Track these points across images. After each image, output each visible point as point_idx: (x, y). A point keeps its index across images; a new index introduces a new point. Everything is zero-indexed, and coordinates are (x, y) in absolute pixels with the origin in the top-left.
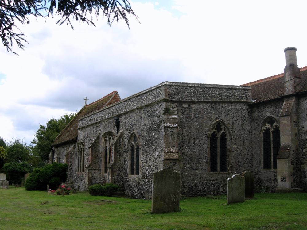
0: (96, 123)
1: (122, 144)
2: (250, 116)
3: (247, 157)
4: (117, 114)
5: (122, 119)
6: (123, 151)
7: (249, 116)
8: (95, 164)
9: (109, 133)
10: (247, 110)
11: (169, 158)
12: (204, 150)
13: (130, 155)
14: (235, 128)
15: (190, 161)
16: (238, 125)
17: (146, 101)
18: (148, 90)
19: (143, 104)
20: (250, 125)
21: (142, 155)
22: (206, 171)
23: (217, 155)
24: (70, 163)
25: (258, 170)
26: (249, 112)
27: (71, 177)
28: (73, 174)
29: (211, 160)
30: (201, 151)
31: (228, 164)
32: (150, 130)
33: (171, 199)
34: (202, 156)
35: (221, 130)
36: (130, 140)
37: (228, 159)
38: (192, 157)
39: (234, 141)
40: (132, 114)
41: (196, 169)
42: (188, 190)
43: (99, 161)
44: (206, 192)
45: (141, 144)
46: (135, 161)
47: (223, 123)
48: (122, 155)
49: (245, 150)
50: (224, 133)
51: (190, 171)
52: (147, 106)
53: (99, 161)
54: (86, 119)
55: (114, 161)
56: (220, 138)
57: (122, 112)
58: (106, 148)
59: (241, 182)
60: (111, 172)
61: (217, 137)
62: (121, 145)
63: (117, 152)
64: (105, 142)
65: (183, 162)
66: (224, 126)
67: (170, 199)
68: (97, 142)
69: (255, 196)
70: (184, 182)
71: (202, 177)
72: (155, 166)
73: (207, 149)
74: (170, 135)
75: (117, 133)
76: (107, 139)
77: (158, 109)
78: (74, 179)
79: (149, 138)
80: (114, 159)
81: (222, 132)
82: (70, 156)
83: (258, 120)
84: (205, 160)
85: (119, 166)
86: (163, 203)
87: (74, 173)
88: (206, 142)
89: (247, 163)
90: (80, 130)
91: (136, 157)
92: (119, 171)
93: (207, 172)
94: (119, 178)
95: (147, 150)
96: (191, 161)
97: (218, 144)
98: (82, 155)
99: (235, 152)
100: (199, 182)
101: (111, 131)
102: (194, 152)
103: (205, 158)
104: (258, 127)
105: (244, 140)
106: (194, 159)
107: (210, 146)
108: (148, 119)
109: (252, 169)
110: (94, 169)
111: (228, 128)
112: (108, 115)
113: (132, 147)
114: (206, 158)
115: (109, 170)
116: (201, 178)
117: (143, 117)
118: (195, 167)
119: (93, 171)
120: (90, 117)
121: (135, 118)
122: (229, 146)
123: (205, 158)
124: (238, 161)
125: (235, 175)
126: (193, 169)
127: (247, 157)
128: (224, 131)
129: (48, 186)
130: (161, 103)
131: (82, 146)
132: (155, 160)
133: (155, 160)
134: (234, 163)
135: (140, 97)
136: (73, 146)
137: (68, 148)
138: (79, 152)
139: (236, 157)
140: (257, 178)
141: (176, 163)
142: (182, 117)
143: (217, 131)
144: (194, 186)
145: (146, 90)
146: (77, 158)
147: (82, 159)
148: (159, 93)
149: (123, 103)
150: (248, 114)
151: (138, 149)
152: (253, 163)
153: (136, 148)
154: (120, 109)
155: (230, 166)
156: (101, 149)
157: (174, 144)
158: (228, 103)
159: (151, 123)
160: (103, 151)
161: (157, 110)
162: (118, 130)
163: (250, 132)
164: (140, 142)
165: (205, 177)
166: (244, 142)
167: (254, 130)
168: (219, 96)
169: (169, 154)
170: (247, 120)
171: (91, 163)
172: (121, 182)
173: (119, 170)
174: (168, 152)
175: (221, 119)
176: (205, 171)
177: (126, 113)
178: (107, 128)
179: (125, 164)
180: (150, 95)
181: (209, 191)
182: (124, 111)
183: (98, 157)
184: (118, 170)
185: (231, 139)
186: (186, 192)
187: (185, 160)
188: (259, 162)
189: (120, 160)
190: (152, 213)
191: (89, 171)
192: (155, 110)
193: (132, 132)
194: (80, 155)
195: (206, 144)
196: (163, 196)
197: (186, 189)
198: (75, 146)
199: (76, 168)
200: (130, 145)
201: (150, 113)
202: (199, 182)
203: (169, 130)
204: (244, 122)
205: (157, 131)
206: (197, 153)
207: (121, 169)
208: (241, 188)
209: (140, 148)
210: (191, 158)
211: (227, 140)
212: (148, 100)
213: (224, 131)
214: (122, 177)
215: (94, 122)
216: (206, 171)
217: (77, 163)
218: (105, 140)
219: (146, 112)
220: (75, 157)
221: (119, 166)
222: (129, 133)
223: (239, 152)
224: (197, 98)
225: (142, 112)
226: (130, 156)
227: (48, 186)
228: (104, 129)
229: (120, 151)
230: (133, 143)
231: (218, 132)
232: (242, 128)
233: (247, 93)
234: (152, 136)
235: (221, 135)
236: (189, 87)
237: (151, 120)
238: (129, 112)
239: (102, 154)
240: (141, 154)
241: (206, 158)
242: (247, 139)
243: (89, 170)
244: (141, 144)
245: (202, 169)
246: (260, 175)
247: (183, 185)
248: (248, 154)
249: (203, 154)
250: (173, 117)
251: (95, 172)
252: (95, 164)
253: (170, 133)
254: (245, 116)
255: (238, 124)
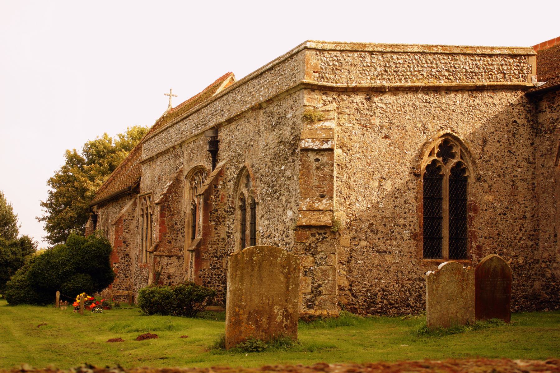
0: (174, 147)
1: (221, 193)
2: (532, 120)
3: (522, 224)
4: (212, 124)
5: (223, 135)
6: (225, 210)
7: (528, 121)
8: (170, 242)
9: (199, 171)
10: (524, 106)
11: (308, 223)
12: (407, 205)
13: (239, 220)
14: (489, 153)
15: (369, 233)
16: (498, 144)
17: (269, 90)
18: (271, 64)
19: (262, 97)
20: (532, 144)
21: (261, 218)
22: (411, 257)
23: (441, 218)
24: (125, 242)
25: (549, 255)
26: (529, 112)
27: (128, 275)
28: (131, 269)
29: (425, 231)
30: (398, 209)
31: (469, 240)
32: (276, 157)
33: (290, 321)
34: (402, 221)
35: (453, 156)
36: (237, 184)
37: (470, 229)
38: (375, 223)
39: (486, 185)
40: (243, 122)
41: (385, 252)
42: (365, 302)
43: (180, 235)
44: (412, 307)
45: (258, 192)
46: (248, 232)
47: (457, 139)
48: (223, 221)
49: (517, 206)
50: (459, 164)
51: (369, 257)
52: (269, 101)
53: (180, 235)
54: (156, 138)
55: (203, 233)
56: (450, 177)
57: (222, 120)
58: (194, 205)
59: (462, 280)
60: (196, 261)
61: (441, 173)
62: (220, 198)
63: (211, 213)
64: (192, 190)
65: (351, 235)
66: (459, 147)
67: (271, 318)
68: (176, 192)
69: (513, 319)
70: (353, 282)
71: (401, 272)
72: (286, 245)
73: (415, 204)
74: (314, 168)
75: (213, 169)
76: (196, 184)
77: (292, 108)
78: (132, 280)
79: (274, 179)
80: (203, 230)
81: (455, 161)
82: (124, 227)
83: (551, 132)
84: (408, 230)
85: (214, 247)
86: (253, 326)
87: (135, 265)
88: (411, 185)
89: (521, 238)
90: (146, 165)
91: (251, 223)
92: (215, 259)
93: (412, 259)
94: (215, 274)
95: (271, 207)
96: (372, 231)
97: (444, 191)
98: (149, 222)
99: (488, 212)
100: (392, 284)
101: (202, 164)
102: (380, 211)
103: (410, 225)
104: (551, 149)
105: (513, 181)
106: (381, 228)
107: (421, 197)
108: (272, 133)
109: (536, 252)
110: (167, 254)
111: (469, 152)
112: (198, 127)
113: (243, 200)
114: (412, 224)
115: (192, 255)
116: (399, 274)
117: (262, 129)
118: (382, 247)
119: (165, 260)
120: (164, 134)
121: (248, 130)
122: (474, 195)
123: (410, 225)
124: (498, 234)
125: (446, 263)
126: (378, 252)
127: (522, 224)
128: (460, 159)
129: (58, 294)
130: (298, 93)
131: (148, 202)
132: (285, 230)
133: (285, 230)
134: (485, 238)
135: (257, 81)
136: (131, 202)
137: (121, 208)
138: (142, 215)
139: (492, 223)
140: (549, 276)
141: (326, 236)
142: (350, 125)
143: (440, 159)
144: (379, 293)
145: (268, 65)
146: (140, 230)
147: (149, 232)
148: (293, 70)
149: (225, 97)
150: (526, 118)
151: (254, 206)
152: (539, 240)
153: (251, 204)
154: (219, 111)
155: (475, 246)
156: (183, 209)
157: (324, 191)
158: (470, 90)
159: (277, 141)
160: (187, 212)
161: (291, 110)
162: (215, 162)
163: (532, 160)
164: (256, 187)
165: (409, 273)
166: (514, 186)
167: (542, 156)
168: (447, 74)
169: (309, 215)
170: (524, 132)
171: (160, 241)
172: (220, 283)
173: (217, 257)
174: (308, 210)
175: (453, 131)
176: (408, 257)
177: (229, 121)
178: (195, 159)
179: (229, 242)
180: (275, 75)
181: (418, 305)
182: (227, 116)
183: (176, 227)
184: (212, 257)
185: (478, 179)
186: (358, 306)
187: (356, 231)
188: (552, 235)
189: (217, 233)
190: (210, 349)
191: (155, 259)
192: (285, 111)
193: (241, 166)
194: (145, 224)
195: (413, 191)
196: (255, 310)
197: (360, 301)
198: (135, 204)
199: (138, 254)
200: (238, 196)
201: (276, 118)
202: (392, 284)
203: (312, 156)
204: (514, 136)
205: (290, 159)
206: (388, 213)
207: (219, 254)
208: (463, 294)
209: (258, 203)
210: (372, 224)
211: (469, 180)
212: (272, 88)
213: (460, 159)
214: (222, 271)
215: (171, 145)
216: (411, 257)
217: (140, 242)
218: (191, 187)
219: (269, 116)
220: (136, 228)
221: (214, 247)
222: (237, 167)
223: (499, 210)
224: (389, 79)
225: (261, 116)
226: (240, 223)
227: (58, 294)
228: (190, 160)
229: (217, 210)
230: (244, 191)
231: (445, 161)
232: (509, 151)
233: (525, 65)
234: (280, 173)
235: (452, 169)
236: (368, 52)
237: (278, 135)
238: (234, 117)
239: (186, 220)
240: (258, 217)
241: (412, 224)
242: (522, 180)
243: (154, 258)
244: (258, 192)
245: (400, 252)
246: (555, 269)
247: (350, 290)
248: (524, 217)
249: (404, 216)
250: (322, 126)
251: (170, 261)
252: (170, 242)
253: (314, 165)
254: (518, 121)
255: (499, 142)
